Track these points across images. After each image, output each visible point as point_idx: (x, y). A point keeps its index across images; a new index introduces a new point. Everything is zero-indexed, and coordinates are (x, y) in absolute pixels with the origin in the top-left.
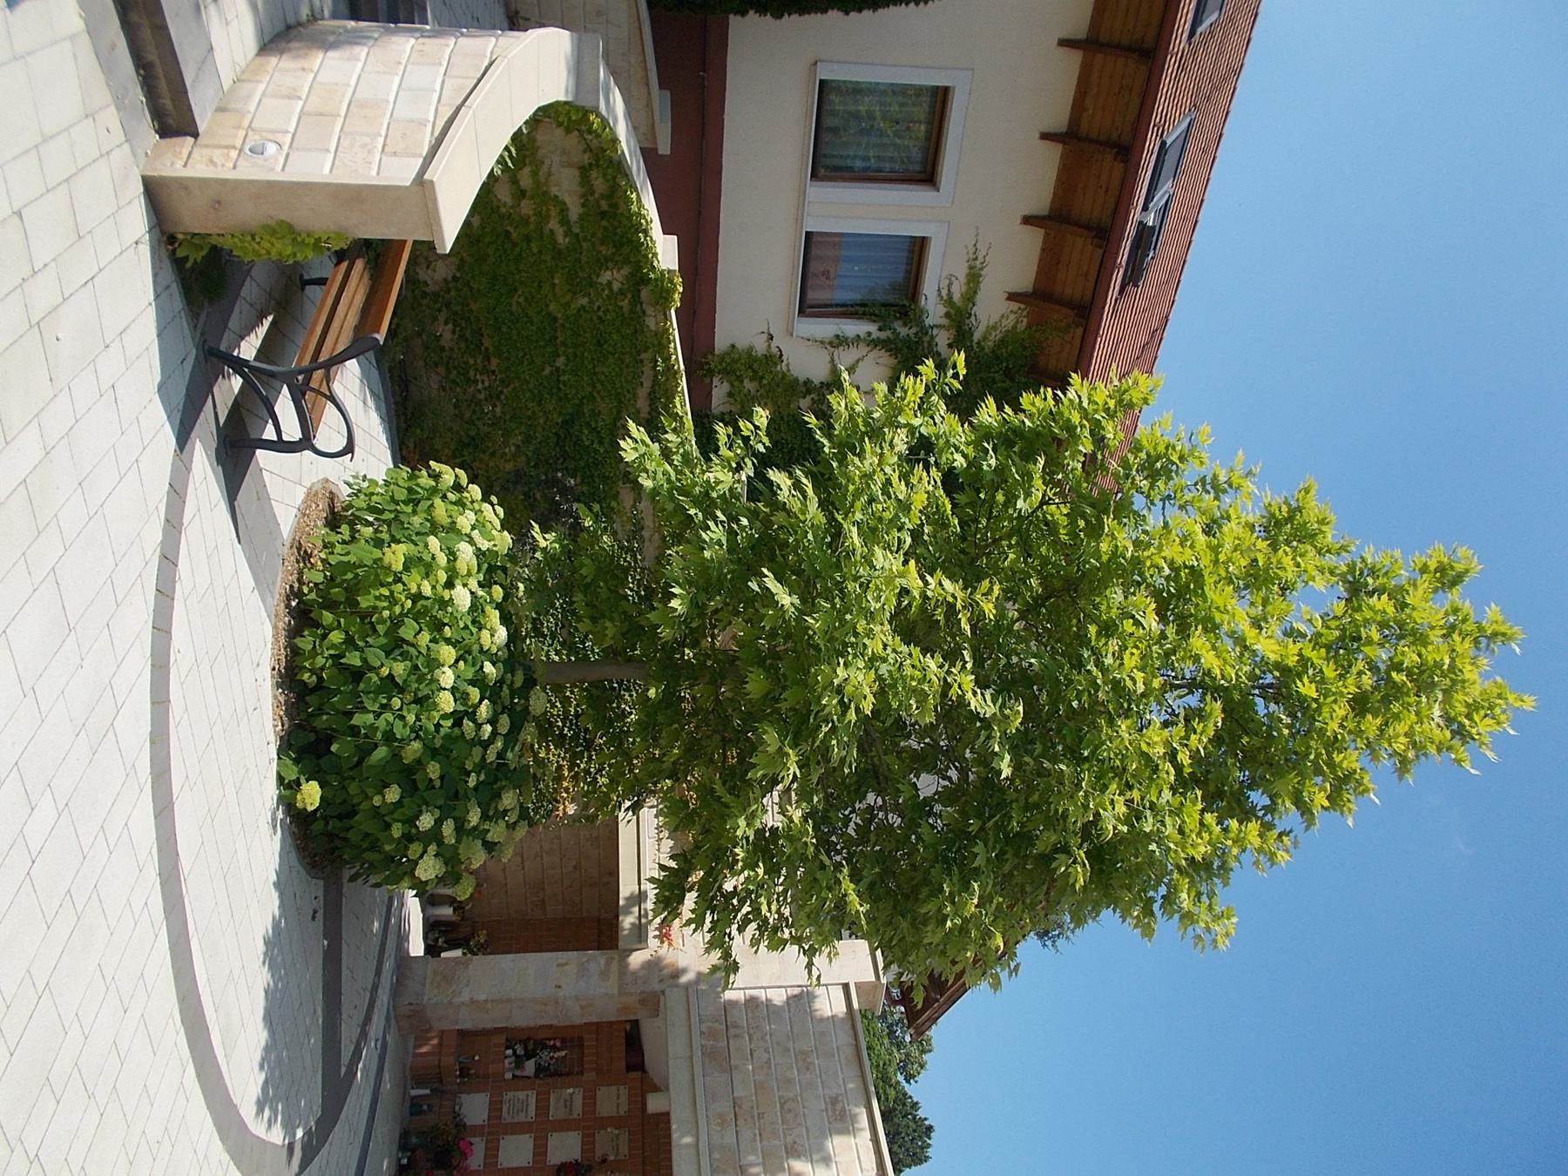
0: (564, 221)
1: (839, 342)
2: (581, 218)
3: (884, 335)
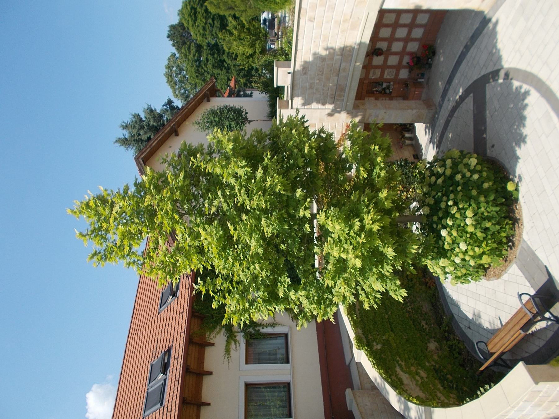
0: (400, 366)
1: (273, 325)
2: (395, 367)
3: (257, 328)
